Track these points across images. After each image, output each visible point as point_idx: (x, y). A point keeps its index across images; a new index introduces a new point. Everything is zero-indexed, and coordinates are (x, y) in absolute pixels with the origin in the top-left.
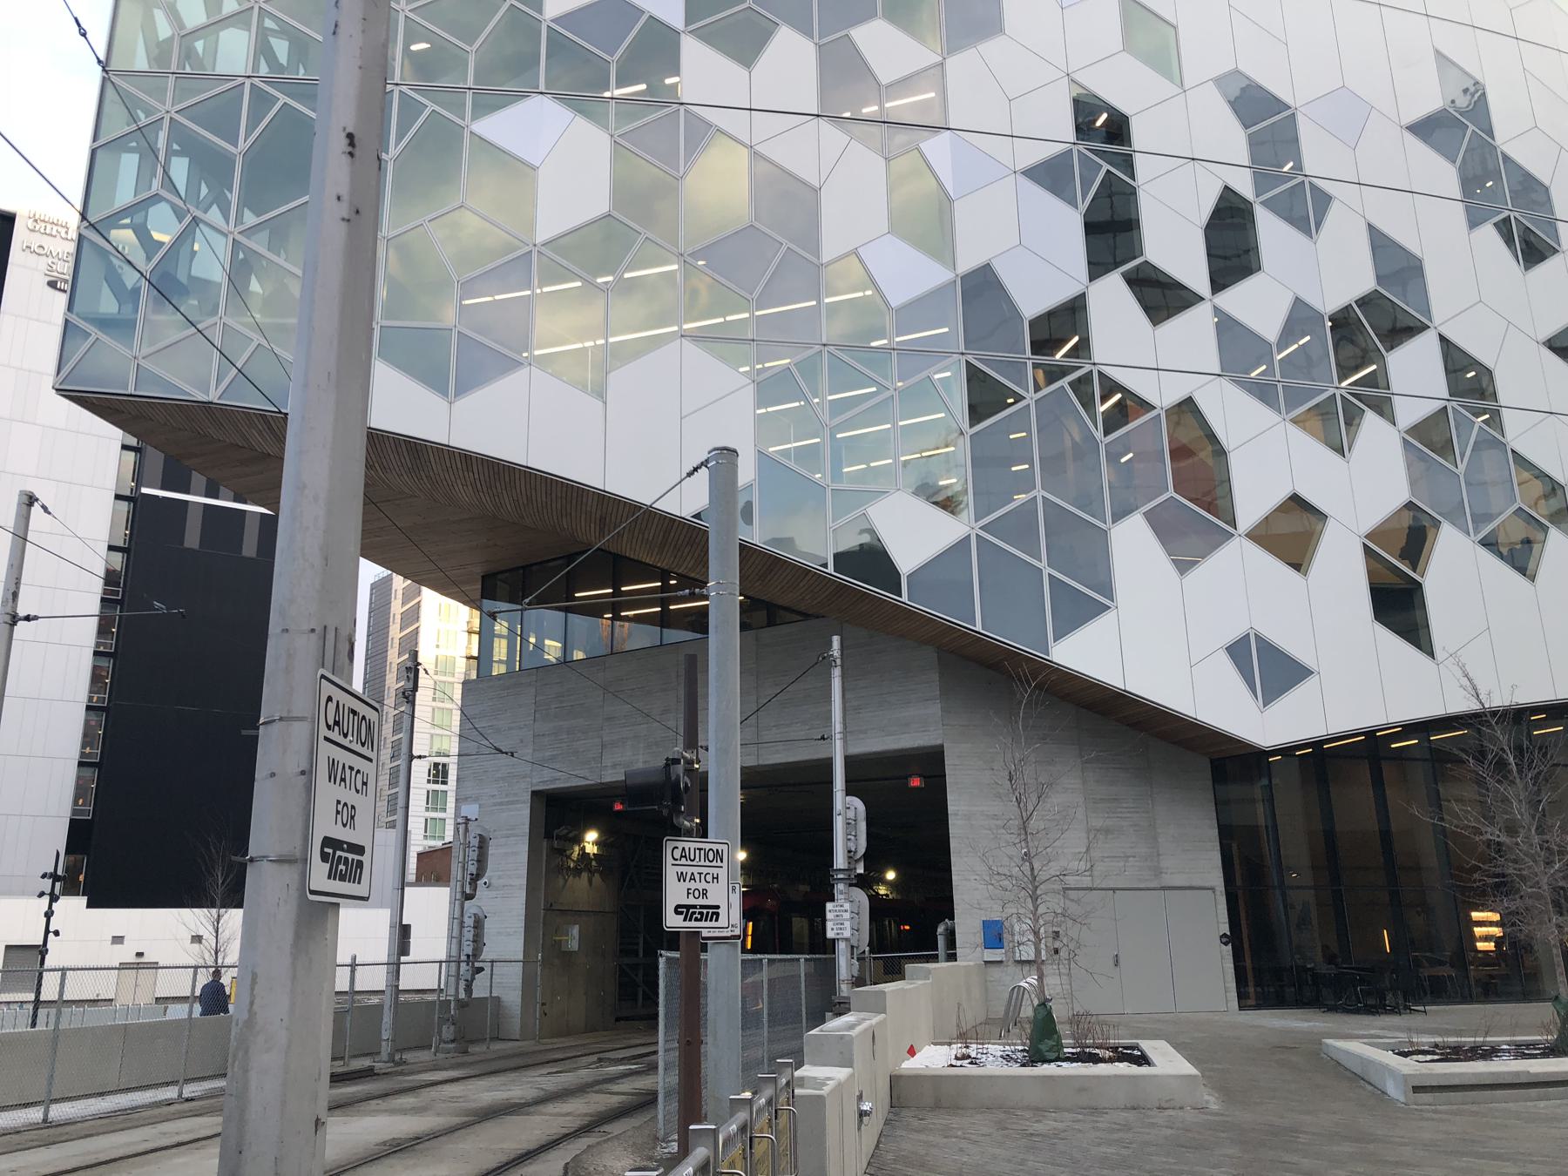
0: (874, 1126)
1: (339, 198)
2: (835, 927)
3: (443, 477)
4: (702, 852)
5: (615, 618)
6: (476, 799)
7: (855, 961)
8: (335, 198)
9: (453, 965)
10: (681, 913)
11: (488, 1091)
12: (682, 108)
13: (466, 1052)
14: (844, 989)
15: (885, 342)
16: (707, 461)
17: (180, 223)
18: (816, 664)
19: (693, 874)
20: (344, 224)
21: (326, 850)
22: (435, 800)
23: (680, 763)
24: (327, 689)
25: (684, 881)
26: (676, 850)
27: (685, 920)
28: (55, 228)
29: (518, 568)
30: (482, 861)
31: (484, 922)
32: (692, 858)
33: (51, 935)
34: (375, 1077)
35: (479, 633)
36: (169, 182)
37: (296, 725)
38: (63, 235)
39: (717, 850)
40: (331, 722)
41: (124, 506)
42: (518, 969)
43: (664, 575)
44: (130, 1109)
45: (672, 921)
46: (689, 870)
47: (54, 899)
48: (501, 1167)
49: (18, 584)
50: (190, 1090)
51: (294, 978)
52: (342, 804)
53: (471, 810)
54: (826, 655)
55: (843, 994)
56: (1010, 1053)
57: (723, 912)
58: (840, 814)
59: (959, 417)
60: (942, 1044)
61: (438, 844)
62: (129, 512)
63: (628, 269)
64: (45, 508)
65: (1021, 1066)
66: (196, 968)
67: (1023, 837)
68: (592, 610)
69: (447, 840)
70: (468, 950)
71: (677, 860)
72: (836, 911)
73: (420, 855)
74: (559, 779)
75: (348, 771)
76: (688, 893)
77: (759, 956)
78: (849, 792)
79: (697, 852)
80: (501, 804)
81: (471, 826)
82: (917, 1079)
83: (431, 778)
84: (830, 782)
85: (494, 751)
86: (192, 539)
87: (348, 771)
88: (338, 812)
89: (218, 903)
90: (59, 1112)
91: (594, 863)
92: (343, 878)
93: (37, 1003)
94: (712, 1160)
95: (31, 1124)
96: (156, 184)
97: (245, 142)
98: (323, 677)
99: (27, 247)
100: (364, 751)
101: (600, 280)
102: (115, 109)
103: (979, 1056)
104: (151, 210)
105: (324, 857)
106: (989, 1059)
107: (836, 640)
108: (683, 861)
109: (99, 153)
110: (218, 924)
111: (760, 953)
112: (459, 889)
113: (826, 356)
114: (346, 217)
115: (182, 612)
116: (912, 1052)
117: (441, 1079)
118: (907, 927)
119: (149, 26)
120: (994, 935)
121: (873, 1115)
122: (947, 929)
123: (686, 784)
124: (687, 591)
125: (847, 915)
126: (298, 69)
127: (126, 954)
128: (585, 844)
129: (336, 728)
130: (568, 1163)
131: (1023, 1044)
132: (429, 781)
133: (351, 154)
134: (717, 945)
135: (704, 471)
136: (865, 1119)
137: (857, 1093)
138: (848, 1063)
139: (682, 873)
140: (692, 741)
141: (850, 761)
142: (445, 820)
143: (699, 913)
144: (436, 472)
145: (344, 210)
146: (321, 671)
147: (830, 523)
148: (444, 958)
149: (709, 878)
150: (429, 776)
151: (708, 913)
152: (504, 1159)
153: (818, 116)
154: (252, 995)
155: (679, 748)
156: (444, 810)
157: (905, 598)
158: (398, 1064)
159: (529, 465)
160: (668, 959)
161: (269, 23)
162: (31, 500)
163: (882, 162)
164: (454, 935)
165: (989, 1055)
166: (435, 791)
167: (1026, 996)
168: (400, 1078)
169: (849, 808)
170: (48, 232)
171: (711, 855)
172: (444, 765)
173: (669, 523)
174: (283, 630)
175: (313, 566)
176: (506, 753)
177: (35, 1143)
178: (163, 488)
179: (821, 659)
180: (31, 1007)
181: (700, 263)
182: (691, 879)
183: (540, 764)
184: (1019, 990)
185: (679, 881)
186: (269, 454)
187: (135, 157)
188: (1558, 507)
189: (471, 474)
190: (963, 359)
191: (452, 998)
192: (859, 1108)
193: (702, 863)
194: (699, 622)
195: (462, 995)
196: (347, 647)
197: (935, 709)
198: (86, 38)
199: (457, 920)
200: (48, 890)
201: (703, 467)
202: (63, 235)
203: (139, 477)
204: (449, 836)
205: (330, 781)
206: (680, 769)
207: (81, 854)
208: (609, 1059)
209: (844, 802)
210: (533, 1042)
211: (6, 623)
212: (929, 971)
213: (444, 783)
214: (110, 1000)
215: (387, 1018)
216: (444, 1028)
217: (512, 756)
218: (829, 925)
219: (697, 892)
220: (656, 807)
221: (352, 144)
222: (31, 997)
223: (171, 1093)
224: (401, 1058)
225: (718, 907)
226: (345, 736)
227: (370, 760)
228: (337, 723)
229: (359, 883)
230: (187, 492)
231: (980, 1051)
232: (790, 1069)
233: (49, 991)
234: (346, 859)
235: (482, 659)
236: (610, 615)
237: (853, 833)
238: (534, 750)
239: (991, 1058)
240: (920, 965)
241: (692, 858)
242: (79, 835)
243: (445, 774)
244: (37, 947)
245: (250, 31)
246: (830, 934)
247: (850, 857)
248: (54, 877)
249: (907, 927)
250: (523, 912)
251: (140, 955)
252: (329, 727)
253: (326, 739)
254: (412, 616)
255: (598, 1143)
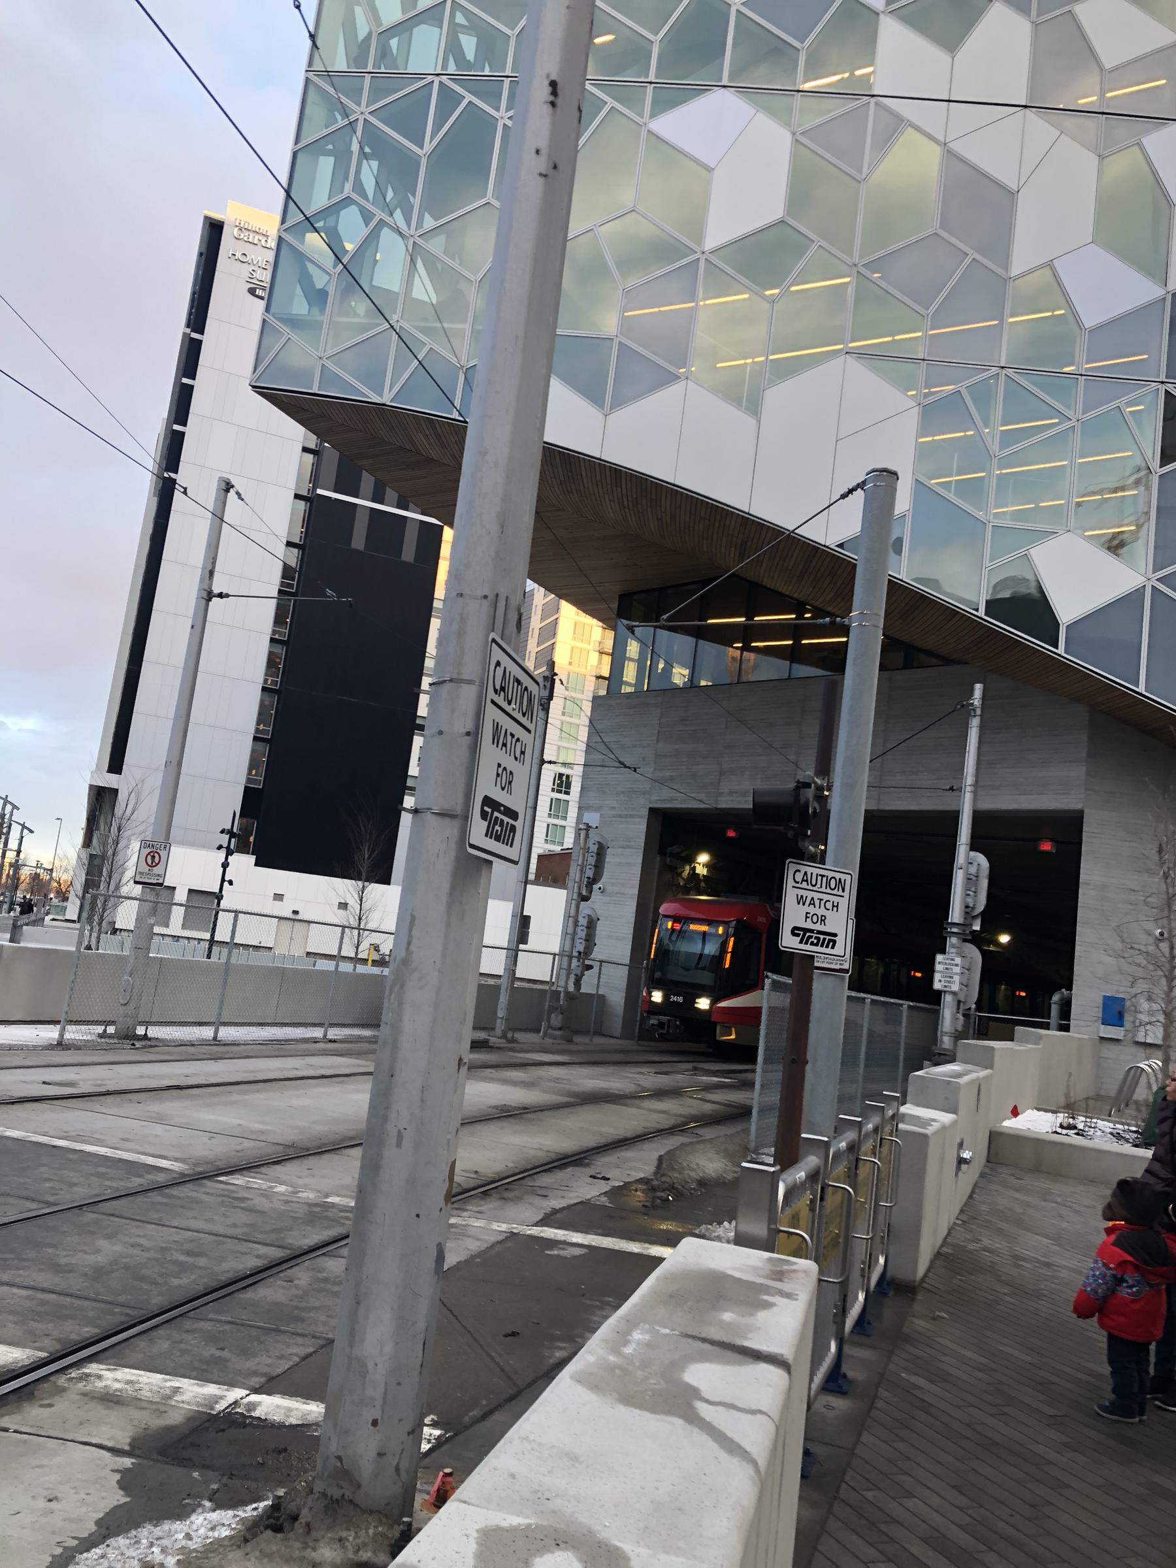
0: (970, 1175)
1: (538, 152)
2: (943, 979)
3: (591, 492)
4: (825, 879)
5: (746, 648)
6: (597, 809)
7: (960, 1016)
8: (533, 151)
9: (565, 959)
10: (798, 935)
11: (590, 1079)
12: (873, 100)
13: (570, 1041)
14: (946, 1042)
15: (1073, 368)
16: (864, 483)
17: (367, 226)
18: (953, 711)
19: (813, 899)
20: (541, 180)
21: (486, 808)
22: (558, 809)
23: (810, 788)
24: (497, 655)
25: (804, 904)
26: (797, 873)
27: (801, 942)
28: (257, 237)
29: (654, 590)
30: (599, 867)
31: (596, 923)
32: (814, 883)
33: (226, 884)
34: (489, 1049)
35: (612, 655)
36: (359, 187)
37: (465, 687)
38: (263, 243)
39: (840, 879)
40: (498, 687)
41: (302, 505)
42: (624, 972)
43: (799, 609)
44: (283, 1040)
45: (788, 941)
46: (810, 895)
47: (229, 853)
48: (600, 1147)
49: (214, 563)
50: (333, 1033)
51: (448, 925)
52: (502, 767)
53: (592, 818)
54: (965, 703)
55: (944, 1046)
56: (1121, 1132)
57: (840, 940)
58: (961, 868)
59: (1149, 454)
60: (1046, 1111)
61: (557, 849)
62: (305, 511)
63: (793, 284)
64: (238, 494)
65: (1133, 1146)
66: (344, 927)
67: (1166, 913)
68: (723, 636)
69: (565, 846)
70: (580, 947)
71: (798, 883)
72: (946, 964)
73: (540, 857)
74: (676, 800)
75: (509, 737)
76: (807, 917)
77: (862, 995)
78: (974, 847)
79: (819, 878)
80: (620, 816)
81: (591, 831)
82: (1019, 1140)
83: (555, 787)
84: (954, 835)
85: (617, 764)
86: (358, 541)
87: (509, 737)
88: (498, 775)
89: (364, 875)
90: (226, 1033)
91: (703, 884)
92: (498, 839)
93: (212, 942)
94: (822, 1172)
95: (203, 1040)
96: (348, 187)
97: (430, 143)
98: (494, 640)
99: (233, 254)
100: (523, 720)
101: (768, 293)
102: (316, 111)
103: (1087, 1129)
104: (343, 213)
105: (484, 815)
106: (1097, 1134)
107: (978, 688)
108: (804, 885)
109: (300, 156)
110: (363, 893)
111: (864, 993)
112: (576, 890)
113: (1002, 379)
114: (544, 172)
115: (350, 601)
116: (1015, 1113)
117: (547, 1061)
118: (1023, 994)
119: (349, 25)
120: (1114, 1012)
121: (972, 1164)
122: (1062, 999)
123: (815, 809)
124: (828, 619)
125: (957, 970)
126: (484, 66)
127: (284, 909)
128: (697, 865)
129: (502, 693)
130: (661, 1156)
131: (1137, 1126)
132: (553, 790)
133: (553, 104)
134: (823, 976)
135: (859, 493)
136: (964, 1167)
137: (959, 1141)
138: (954, 1111)
139: (802, 896)
140: (824, 766)
141: (979, 817)
142: (565, 827)
143: (816, 938)
144: (586, 485)
145: (542, 164)
146: (492, 635)
147: (987, 562)
148: (557, 951)
149: (829, 905)
150: (554, 785)
151: (824, 939)
152: (603, 1141)
153: (1026, 107)
154: (410, 935)
155: (810, 772)
156: (565, 818)
157: (1061, 650)
158: (509, 1041)
159: (677, 483)
160: (774, 981)
161: (460, 19)
162: (228, 486)
163: (1095, 159)
164: (569, 932)
165: (1097, 1129)
166: (558, 800)
167: (1143, 1079)
168: (511, 1053)
169: (971, 863)
170: (250, 240)
171: (833, 883)
172: (568, 777)
173: (813, 552)
174: (458, 594)
175: (490, 533)
176: (629, 768)
177: (206, 1056)
178: (335, 491)
179: (959, 706)
180: (207, 945)
181: (876, 275)
182: (810, 904)
183: (661, 782)
184: (1136, 1072)
185: (799, 903)
186: (433, 459)
187: (331, 160)
188: (458, 1261)
189: (619, 489)
190: (1162, 388)
191: (561, 989)
192: (959, 1155)
193: (823, 889)
194: (835, 660)
195: (571, 988)
196: (516, 617)
197: (1079, 772)
198: (300, 11)
199: (572, 918)
200: (225, 845)
201: (859, 490)
202: (263, 243)
203: (315, 479)
204: (569, 842)
205: (493, 743)
206: (810, 793)
207: (251, 818)
208: (702, 1069)
209: (967, 857)
210: (631, 1042)
211: (203, 598)
212: (1040, 1037)
213: (567, 793)
214: (269, 948)
215: (503, 999)
216: (553, 1016)
217: (635, 771)
218: (937, 976)
219: (815, 917)
220: (782, 828)
221: (554, 93)
222: (207, 936)
223: (318, 1033)
224: (513, 1037)
225: (835, 935)
226: (510, 703)
227: (529, 731)
228: (503, 689)
229: (511, 846)
230: (356, 496)
231: (1089, 1124)
232: (896, 1103)
233: (222, 934)
234: (502, 821)
235: (614, 678)
236: (740, 645)
237: (973, 890)
238: (655, 769)
239: (1099, 1133)
240: (1030, 1029)
241: (814, 883)
242: (252, 800)
243: (568, 785)
244: (213, 893)
245: (441, 28)
246: (937, 986)
247: (967, 913)
248: (231, 834)
249: (1023, 994)
250: (633, 920)
251: (296, 912)
252: (496, 691)
253: (493, 702)
254: (550, 631)
255: (691, 1143)
